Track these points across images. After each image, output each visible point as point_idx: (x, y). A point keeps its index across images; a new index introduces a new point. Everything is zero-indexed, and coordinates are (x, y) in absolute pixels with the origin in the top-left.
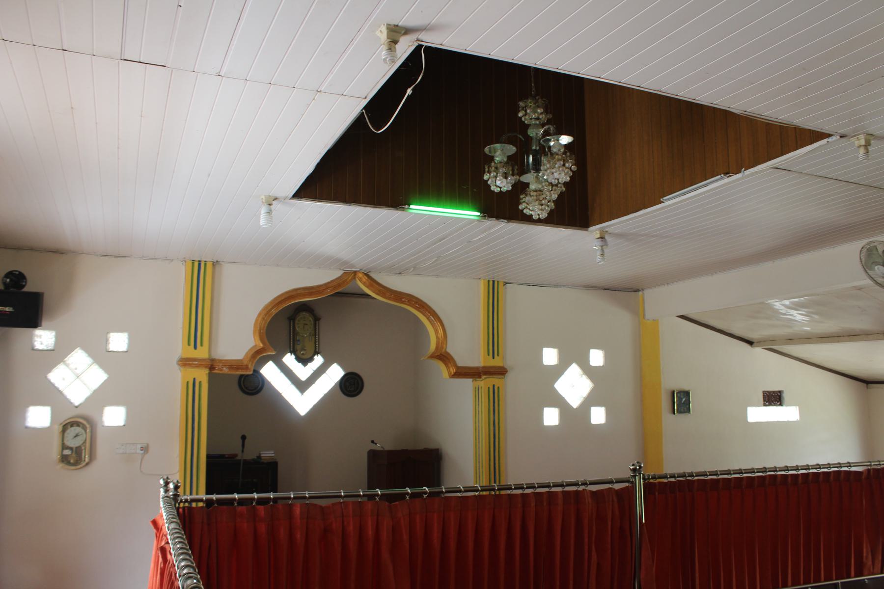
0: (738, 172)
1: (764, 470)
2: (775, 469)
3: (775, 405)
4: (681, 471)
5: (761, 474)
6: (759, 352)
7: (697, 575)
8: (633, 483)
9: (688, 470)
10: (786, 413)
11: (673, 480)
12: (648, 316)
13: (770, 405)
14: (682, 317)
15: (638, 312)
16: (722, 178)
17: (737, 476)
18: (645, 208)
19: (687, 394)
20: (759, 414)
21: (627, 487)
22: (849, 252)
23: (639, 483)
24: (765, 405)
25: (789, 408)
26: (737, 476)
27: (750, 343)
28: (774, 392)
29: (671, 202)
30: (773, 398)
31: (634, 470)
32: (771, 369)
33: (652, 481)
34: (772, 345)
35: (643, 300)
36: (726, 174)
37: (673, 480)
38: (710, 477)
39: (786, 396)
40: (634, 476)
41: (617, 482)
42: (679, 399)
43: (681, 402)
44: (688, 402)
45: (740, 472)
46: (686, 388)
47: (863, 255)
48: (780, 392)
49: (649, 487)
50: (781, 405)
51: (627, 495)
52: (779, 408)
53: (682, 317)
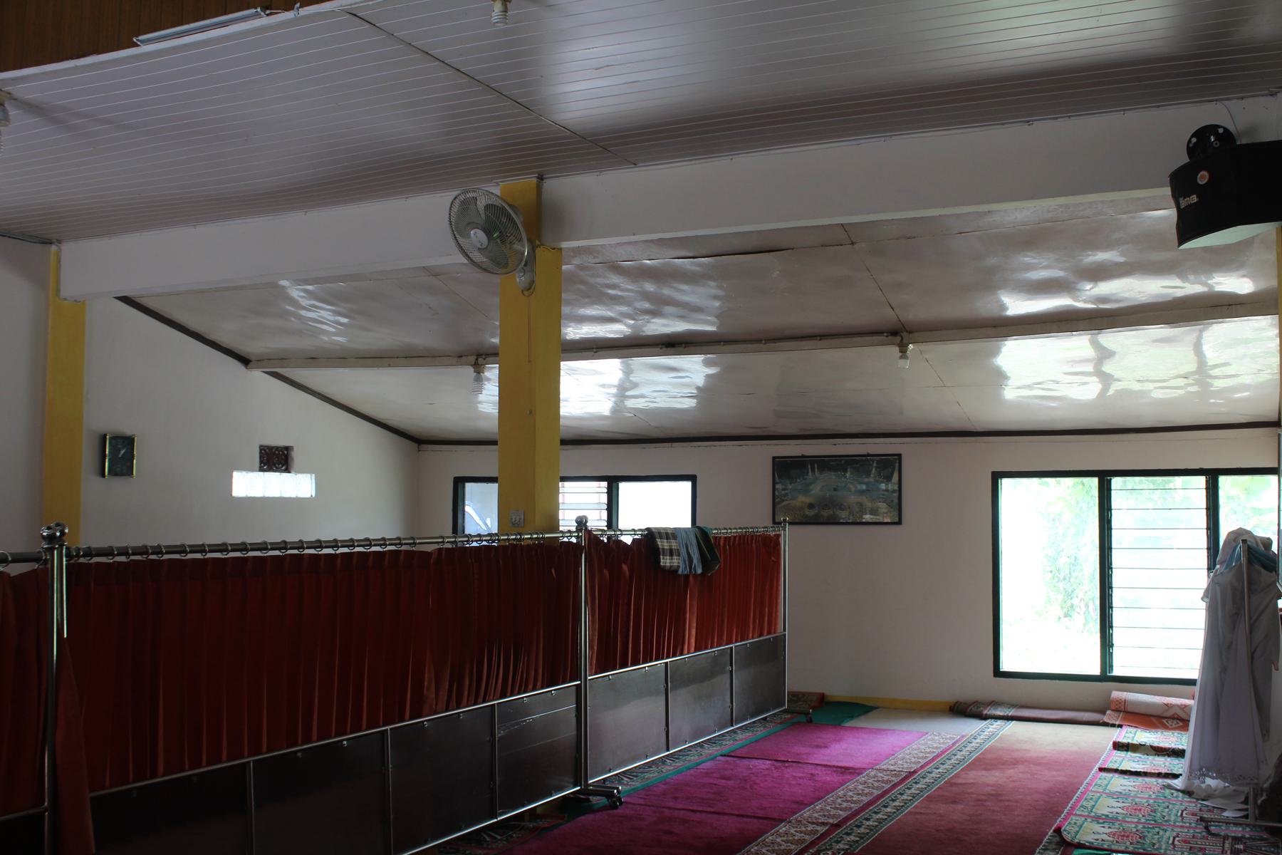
0: (289, 8)
1: (284, 545)
2: (301, 545)
3: (278, 470)
4: (138, 543)
5: (277, 553)
6: (257, 376)
7: (161, 731)
8: (47, 563)
9: (152, 542)
10: (294, 485)
11: (123, 559)
12: (65, 292)
13: (270, 470)
14: (126, 300)
15: (45, 281)
16: (257, 16)
17: (238, 554)
18: (98, 52)
19: (129, 441)
20: (251, 484)
21: (34, 571)
22: (433, 207)
23: (59, 563)
24: (261, 470)
25: (300, 476)
26: (238, 554)
27: (245, 361)
28: (277, 448)
29: (152, 46)
30: (276, 459)
31: (51, 538)
32: (274, 408)
33: (82, 560)
34: (278, 366)
35: (59, 261)
36: (265, 8)
37: (123, 559)
38: (190, 556)
39: (296, 456)
40: (51, 550)
41: (14, 561)
42: (115, 450)
43: (118, 454)
44: (130, 457)
45: (243, 547)
46: (127, 431)
47: (455, 209)
48: (287, 448)
49: (78, 574)
50: (287, 470)
51: (37, 583)
52: (285, 475)
53: (126, 300)
